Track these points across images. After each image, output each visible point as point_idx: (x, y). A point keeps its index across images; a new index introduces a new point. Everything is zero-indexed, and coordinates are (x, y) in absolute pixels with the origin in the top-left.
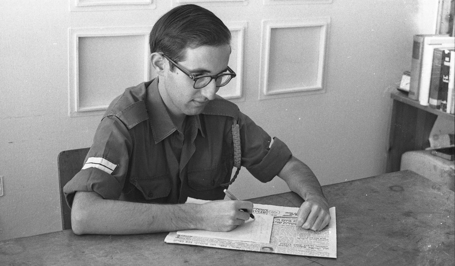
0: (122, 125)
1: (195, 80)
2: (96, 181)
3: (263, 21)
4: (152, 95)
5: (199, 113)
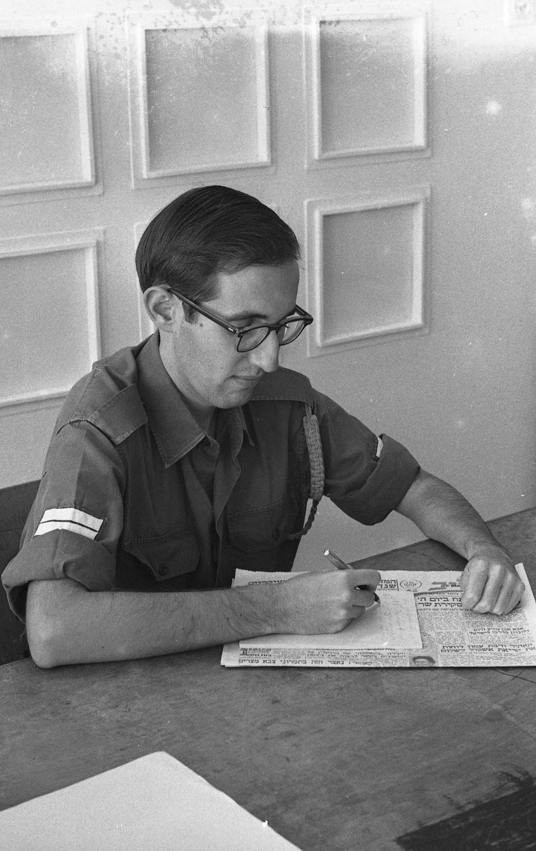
0: (102, 438)
2: (70, 557)
3: (306, 203)
4: (149, 373)
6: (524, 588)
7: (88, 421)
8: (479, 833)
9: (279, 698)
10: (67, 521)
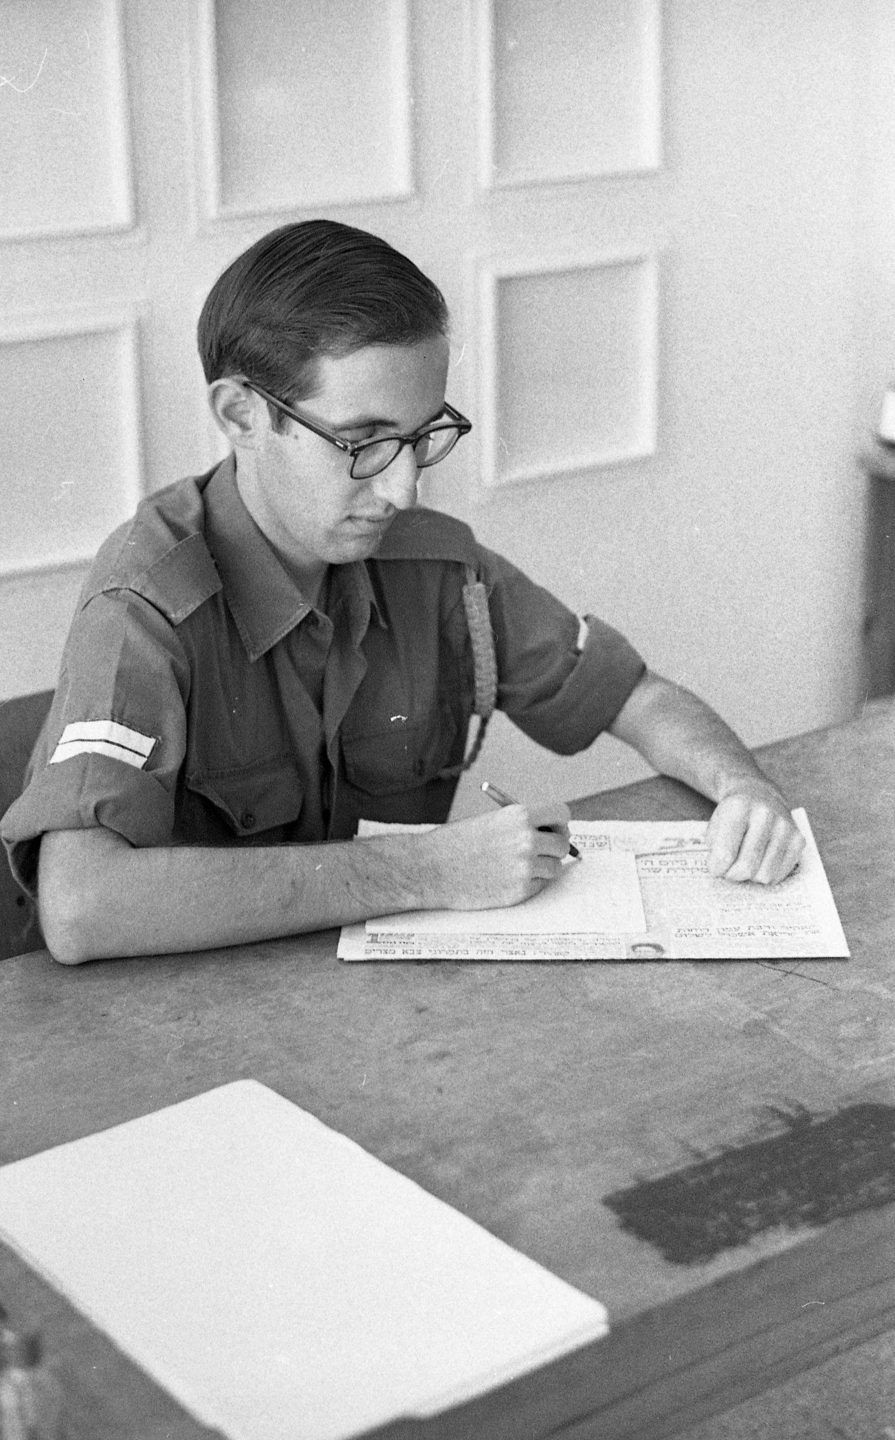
1: (354, 454)
4: (220, 513)
5: (366, 556)
6: (804, 842)
7: (130, 590)
8: (727, 1191)
9: (425, 1003)
10: (101, 740)
